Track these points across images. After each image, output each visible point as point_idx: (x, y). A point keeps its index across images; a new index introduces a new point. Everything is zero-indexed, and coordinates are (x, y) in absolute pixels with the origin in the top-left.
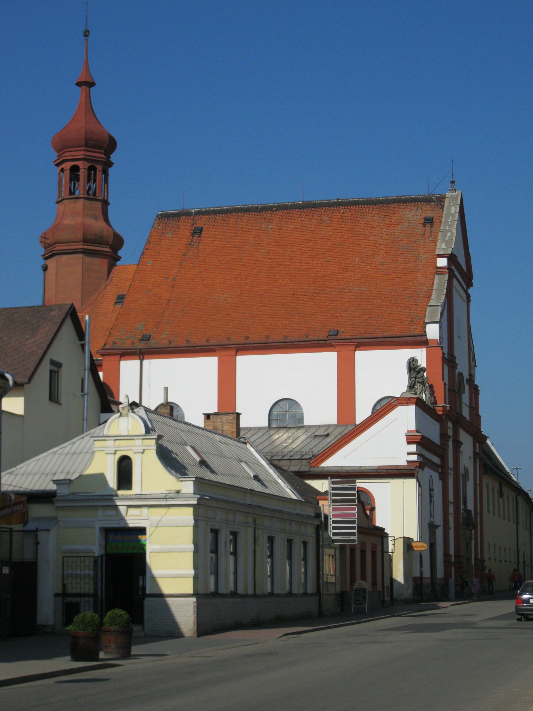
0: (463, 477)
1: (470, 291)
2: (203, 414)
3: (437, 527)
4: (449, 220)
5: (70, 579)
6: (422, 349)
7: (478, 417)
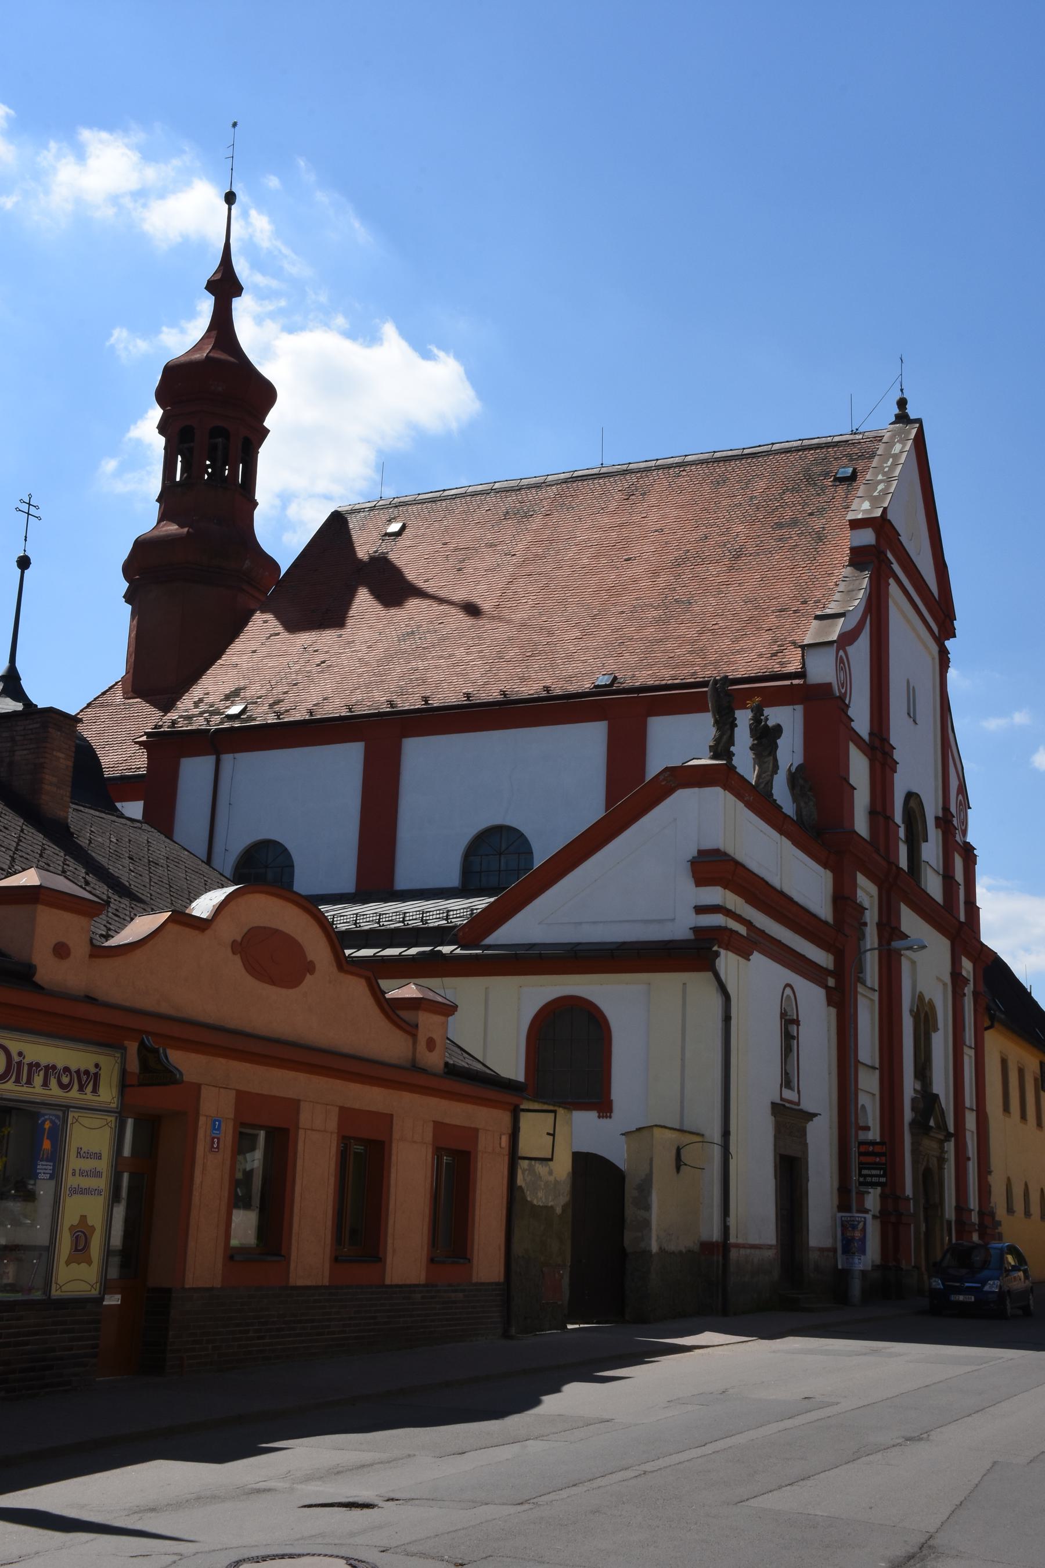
1: (949, 644)
4: (885, 465)
6: (796, 707)
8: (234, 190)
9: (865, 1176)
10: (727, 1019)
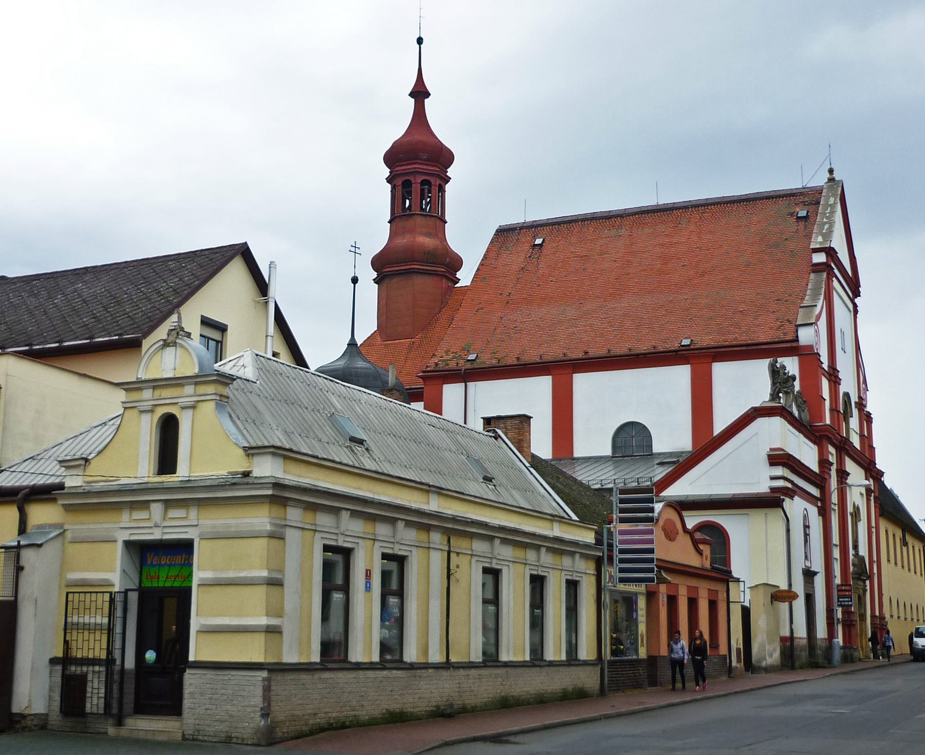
0: (851, 514)
1: (857, 300)
2: (482, 418)
3: (815, 573)
4: (826, 212)
5: (75, 633)
6: (794, 357)
7: (872, 449)
8: (421, 36)
9: (841, 602)
10: (788, 530)
